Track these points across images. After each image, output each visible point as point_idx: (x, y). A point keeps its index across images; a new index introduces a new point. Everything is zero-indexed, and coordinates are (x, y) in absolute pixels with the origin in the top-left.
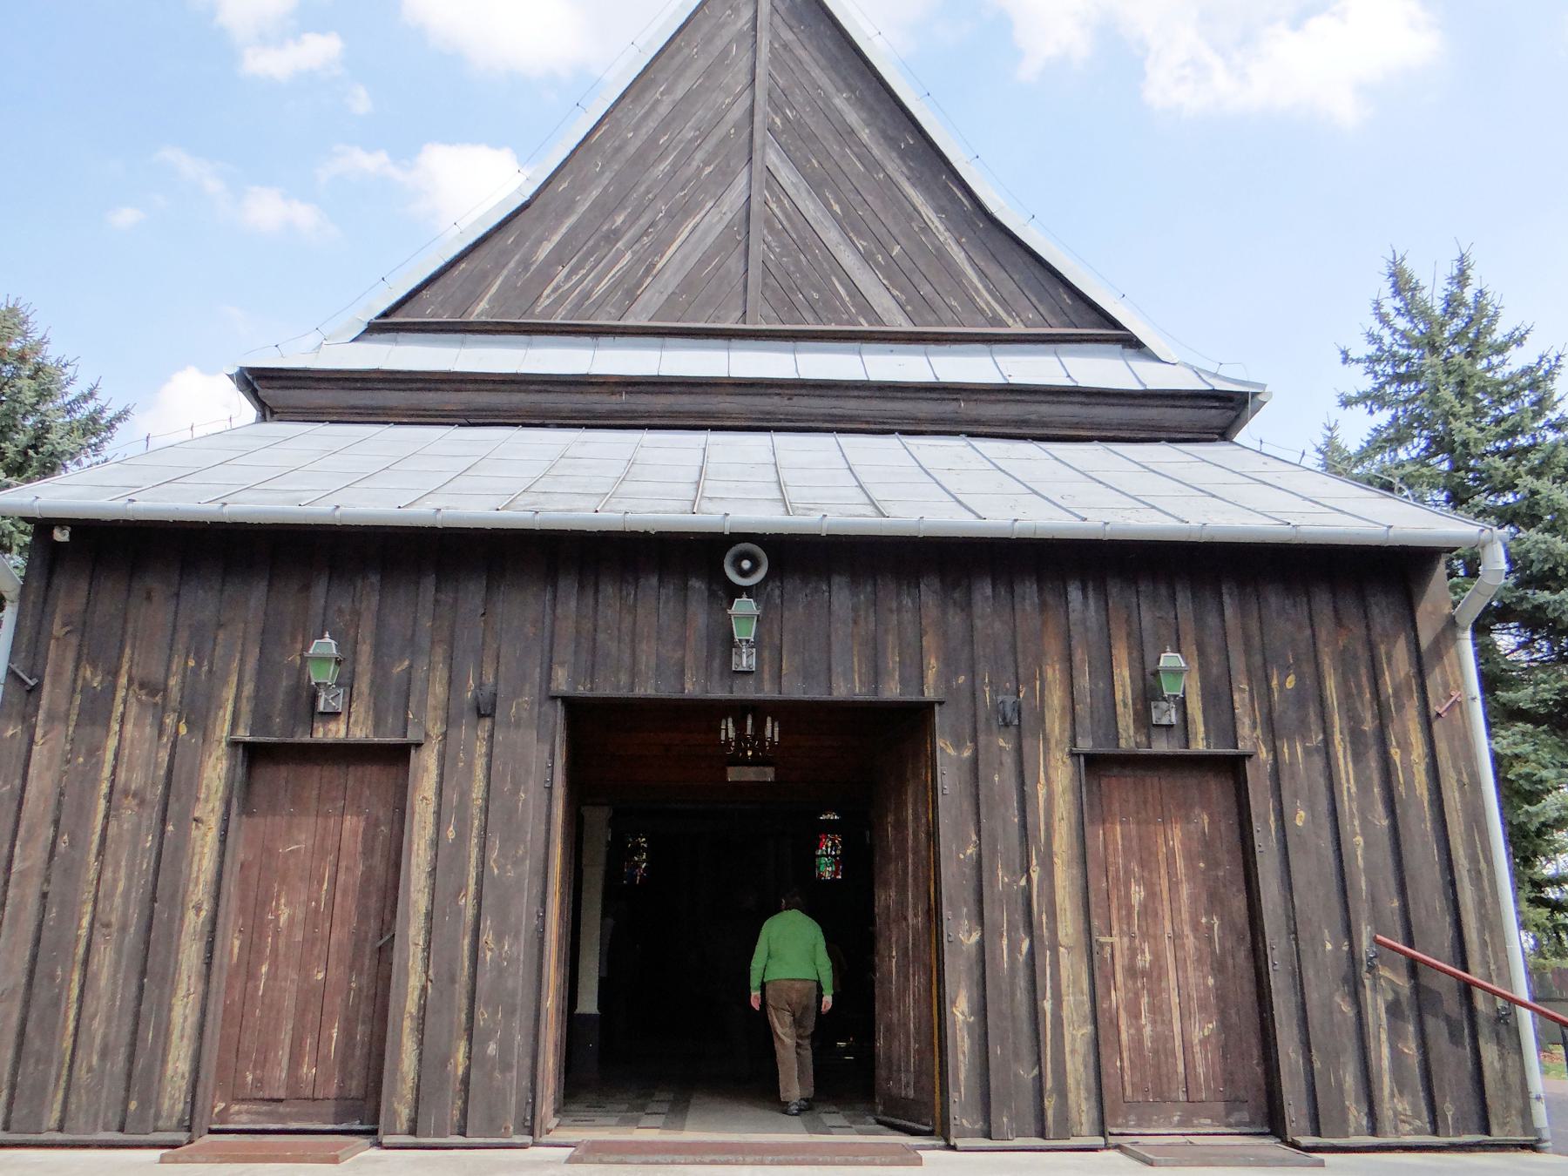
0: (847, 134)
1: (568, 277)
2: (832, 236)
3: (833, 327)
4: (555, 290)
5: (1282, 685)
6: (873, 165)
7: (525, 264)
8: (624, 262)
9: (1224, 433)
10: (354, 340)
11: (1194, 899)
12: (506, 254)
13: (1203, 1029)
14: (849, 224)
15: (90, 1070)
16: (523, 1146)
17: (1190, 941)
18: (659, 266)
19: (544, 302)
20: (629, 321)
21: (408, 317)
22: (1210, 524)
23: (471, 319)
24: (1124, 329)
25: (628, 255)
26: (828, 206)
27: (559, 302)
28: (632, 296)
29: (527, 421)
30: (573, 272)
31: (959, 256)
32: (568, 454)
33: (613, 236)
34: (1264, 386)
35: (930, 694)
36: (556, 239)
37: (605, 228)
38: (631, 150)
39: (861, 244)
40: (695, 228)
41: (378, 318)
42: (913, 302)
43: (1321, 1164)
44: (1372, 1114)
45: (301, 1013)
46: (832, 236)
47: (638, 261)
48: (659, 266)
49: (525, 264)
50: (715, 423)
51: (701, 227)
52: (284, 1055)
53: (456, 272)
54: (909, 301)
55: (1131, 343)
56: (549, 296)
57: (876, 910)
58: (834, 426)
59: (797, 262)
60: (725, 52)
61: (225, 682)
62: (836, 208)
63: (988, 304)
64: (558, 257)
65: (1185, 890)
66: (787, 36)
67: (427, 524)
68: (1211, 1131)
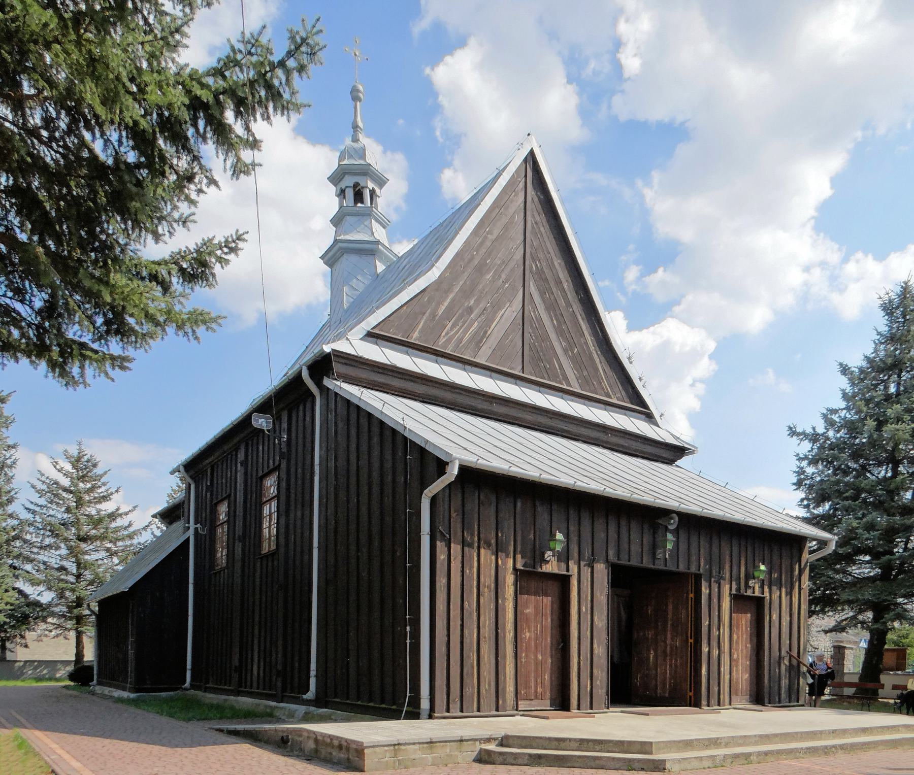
0: (559, 282)
1: (452, 329)
2: (553, 336)
3: (554, 384)
6: (568, 304)
7: (434, 315)
9: (670, 462)
11: (746, 639)
13: (747, 676)
14: (560, 332)
15: (486, 690)
16: (606, 713)
17: (745, 651)
18: (489, 333)
19: (442, 340)
21: (382, 331)
22: (802, 531)
26: (552, 320)
27: (449, 341)
28: (479, 347)
31: (597, 361)
33: (470, 310)
34: (697, 448)
36: (446, 304)
38: (476, 262)
39: (564, 344)
40: (502, 315)
42: (584, 381)
43: (594, 717)
44: (780, 698)
45: (536, 671)
46: (553, 336)
47: (480, 328)
49: (434, 315)
51: (505, 316)
52: (532, 684)
55: (649, 417)
56: (444, 337)
59: (541, 347)
60: (513, 217)
61: (509, 544)
62: (555, 322)
65: (745, 636)
66: (538, 219)
67: (721, 518)
68: (539, 708)
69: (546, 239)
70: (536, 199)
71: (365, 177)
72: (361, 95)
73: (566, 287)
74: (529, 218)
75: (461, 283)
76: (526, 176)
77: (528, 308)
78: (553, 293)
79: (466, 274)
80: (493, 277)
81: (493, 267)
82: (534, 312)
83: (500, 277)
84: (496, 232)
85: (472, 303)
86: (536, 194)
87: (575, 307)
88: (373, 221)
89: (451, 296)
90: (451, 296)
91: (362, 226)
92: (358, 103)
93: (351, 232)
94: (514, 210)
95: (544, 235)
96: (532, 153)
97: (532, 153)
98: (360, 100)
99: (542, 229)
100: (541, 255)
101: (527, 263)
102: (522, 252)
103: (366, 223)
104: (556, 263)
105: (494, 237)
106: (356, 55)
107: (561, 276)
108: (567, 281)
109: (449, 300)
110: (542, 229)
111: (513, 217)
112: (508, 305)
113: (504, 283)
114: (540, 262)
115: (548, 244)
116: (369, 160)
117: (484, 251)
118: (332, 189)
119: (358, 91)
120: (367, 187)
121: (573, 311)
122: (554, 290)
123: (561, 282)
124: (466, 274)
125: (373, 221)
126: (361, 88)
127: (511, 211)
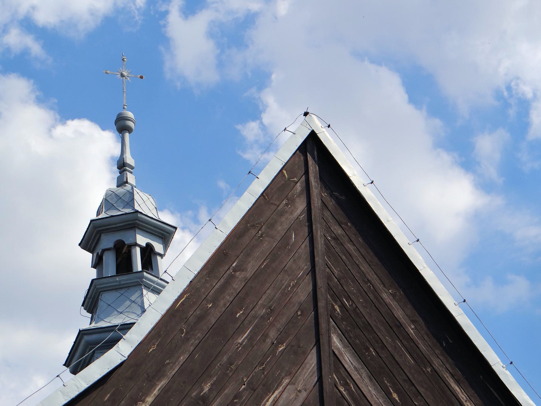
62: (395, 396)
66: (339, 231)
69: (360, 260)
70: (331, 203)
71: (131, 232)
72: (131, 124)
73: (411, 331)
74: (319, 234)
75: (182, 359)
76: (307, 173)
77: (329, 379)
78: (384, 347)
79: (193, 342)
80: (250, 338)
81: (250, 323)
82: (346, 385)
83: (266, 336)
84: (252, 268)
85: (206, 389)
86: (332, 196)
87: (436, 363)
88: (145, 292)
89: (162, 384)
90: (162, 384)
91: (128, 303)
92: (127, 135)
93: (108, 315)
94: (286, 226)
95: (355, 253)
96: (313, 137)
97: (313, 137)
98: (129, 130)
99: (350, 247)
100: (352, 289)
101: (321, 304)
102: (310, 288)
103: (133, 298)
104: (385, 296)
105: (249, 273)
106: (122, 75)
107: (399, 314)
108: (413, 322)
109: (156, 392)
110: (350, 247)
111: (286, 237)
112: (286, 381)
113: (275, 345)
114: (349, 298)
115: (364, 267)
116: (137, 208)
117: (229, 298)
118: (87, 257)
119: (127, 119)
120: (136, 245)
121: (434, 370)
122: (387, 340)
123: (400, 326)
124: (193, 342)
125: (145, 292)
126: (130, 115)
127: (281, 228)
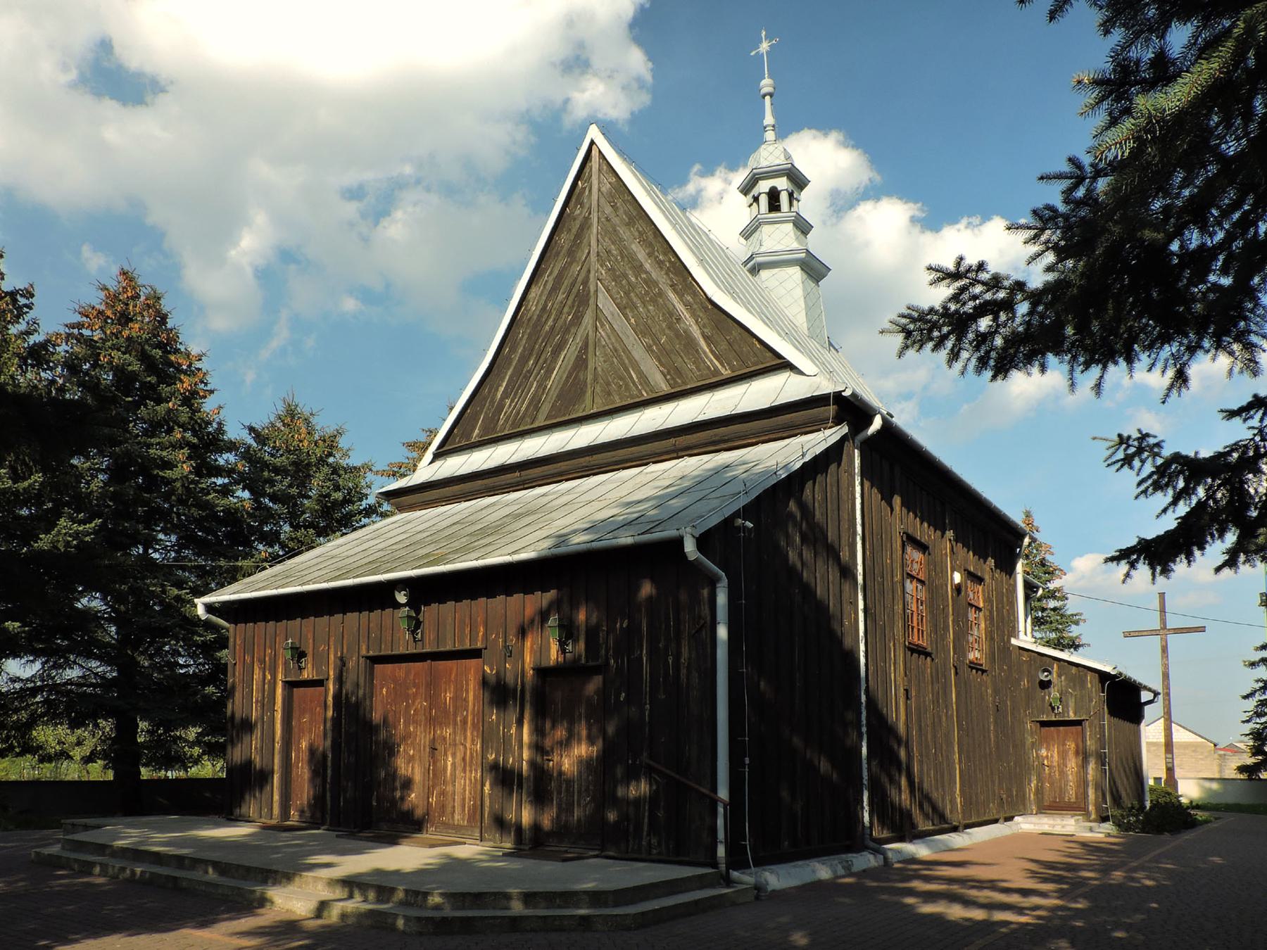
4: (505, 414)
5: (621, 625)
8: (535, 385)
10: (431, 463)
12: (485, 399)
18: (549, 387)
20: (536, 425)
23: (473, 440)
24: (785, 359)
25: (535, 383)
29: (804, 430)
30: (512, 402)
32: (805, 451)
35: (479, 645)
37: (525, 370)
41: (437, 450)
48: (549, 387)
50: (725, 446)
53: (466, 415)
54: (669, 373)
57: (13, 778)
58: (757, 440)
63: (711, 361)
64: (506, 395)
